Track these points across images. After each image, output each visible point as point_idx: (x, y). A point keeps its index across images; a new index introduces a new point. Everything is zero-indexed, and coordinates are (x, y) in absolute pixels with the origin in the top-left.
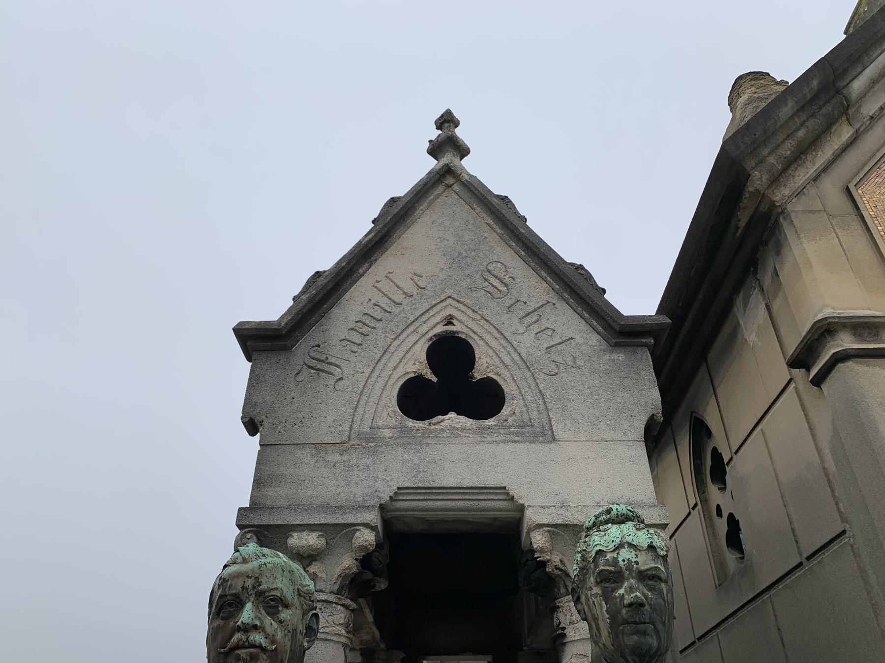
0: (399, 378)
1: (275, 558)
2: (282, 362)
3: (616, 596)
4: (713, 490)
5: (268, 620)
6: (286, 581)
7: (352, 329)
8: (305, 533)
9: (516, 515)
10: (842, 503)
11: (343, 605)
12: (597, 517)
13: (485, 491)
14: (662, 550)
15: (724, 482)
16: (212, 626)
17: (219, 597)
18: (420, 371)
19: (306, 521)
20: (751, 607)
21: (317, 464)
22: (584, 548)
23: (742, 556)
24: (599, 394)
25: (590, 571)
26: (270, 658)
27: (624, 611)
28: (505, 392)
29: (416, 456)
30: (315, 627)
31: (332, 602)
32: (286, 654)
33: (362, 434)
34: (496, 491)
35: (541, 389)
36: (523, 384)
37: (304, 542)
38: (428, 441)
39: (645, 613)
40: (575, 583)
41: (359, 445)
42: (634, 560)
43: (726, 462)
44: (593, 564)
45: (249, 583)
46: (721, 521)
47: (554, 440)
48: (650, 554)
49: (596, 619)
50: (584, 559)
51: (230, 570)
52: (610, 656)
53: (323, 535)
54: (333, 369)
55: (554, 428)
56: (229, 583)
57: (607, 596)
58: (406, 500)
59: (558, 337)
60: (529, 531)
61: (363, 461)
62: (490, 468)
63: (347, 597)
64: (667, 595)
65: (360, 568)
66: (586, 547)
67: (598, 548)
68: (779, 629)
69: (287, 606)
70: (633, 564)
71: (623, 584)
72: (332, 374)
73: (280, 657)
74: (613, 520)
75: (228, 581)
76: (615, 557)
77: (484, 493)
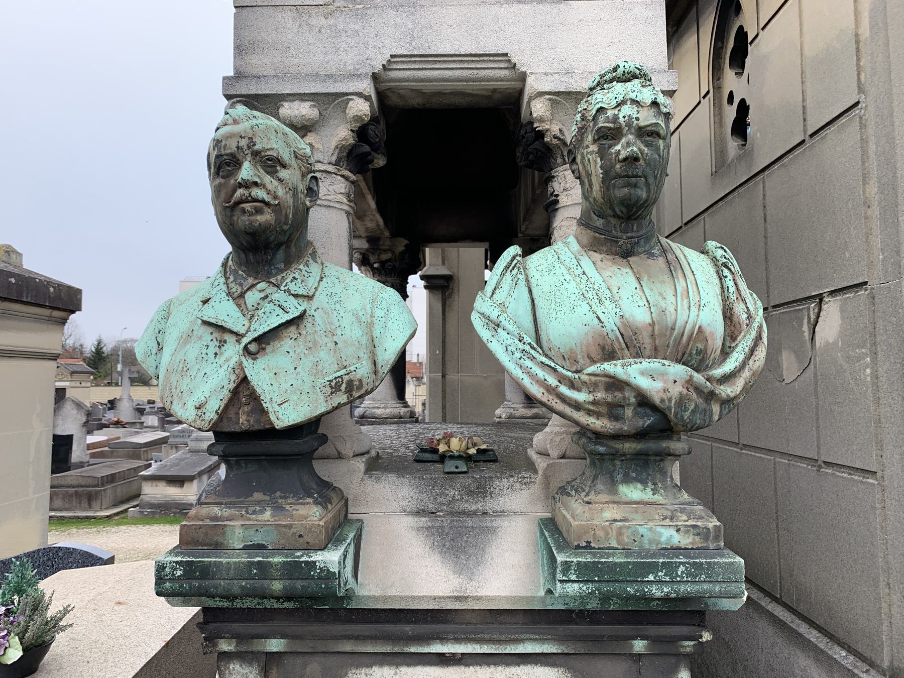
1: (266, 121)
3: (612, 153)
4: (729, 74)
5: (267, 179)
6: (281, 143)
8: (296, 102)
9: (517, 85)
10: (865, 73)
11: (342, 176)
12: (602, 76)
13: (485, 58)
14: (666, 107)
15: (742, 66)
16: (214, 184)
17: (216, 156)
20: (741, 190)
21: (300, 29)
22: (585, 107)
23: (743, 143)
25: (589, 129)
26: (274, 211)
27: (618, 166)
30: (315, 188)
31: (331, 173)
32: (290, 209)
37: (297, 112)
39: (639, 167)
40: (572, 144)
41: (345, 7)
42: (634, 116)
44: (593, 122)
45: (244, 143)
46: (730, 108)
49: (589, 175)
50: (584, 118)
51: (224, 130)
52: (599, 209)
53: (315, 106)
56: (223, 143)
57: (602, 153)
58: (400, 70)
60: (531, 99)
61: (351, 26)
63: (346, 169)
64: (663, 151)
65: (357, 139)
66: (587, 106)
67: (598, 106)
68: (765, 207)
69: (284, 166)
70: (633, 120)
71: (620, 139)
73: (284, 212)
74: (619, 78)
75: (221, 141)
76: (616, 113)
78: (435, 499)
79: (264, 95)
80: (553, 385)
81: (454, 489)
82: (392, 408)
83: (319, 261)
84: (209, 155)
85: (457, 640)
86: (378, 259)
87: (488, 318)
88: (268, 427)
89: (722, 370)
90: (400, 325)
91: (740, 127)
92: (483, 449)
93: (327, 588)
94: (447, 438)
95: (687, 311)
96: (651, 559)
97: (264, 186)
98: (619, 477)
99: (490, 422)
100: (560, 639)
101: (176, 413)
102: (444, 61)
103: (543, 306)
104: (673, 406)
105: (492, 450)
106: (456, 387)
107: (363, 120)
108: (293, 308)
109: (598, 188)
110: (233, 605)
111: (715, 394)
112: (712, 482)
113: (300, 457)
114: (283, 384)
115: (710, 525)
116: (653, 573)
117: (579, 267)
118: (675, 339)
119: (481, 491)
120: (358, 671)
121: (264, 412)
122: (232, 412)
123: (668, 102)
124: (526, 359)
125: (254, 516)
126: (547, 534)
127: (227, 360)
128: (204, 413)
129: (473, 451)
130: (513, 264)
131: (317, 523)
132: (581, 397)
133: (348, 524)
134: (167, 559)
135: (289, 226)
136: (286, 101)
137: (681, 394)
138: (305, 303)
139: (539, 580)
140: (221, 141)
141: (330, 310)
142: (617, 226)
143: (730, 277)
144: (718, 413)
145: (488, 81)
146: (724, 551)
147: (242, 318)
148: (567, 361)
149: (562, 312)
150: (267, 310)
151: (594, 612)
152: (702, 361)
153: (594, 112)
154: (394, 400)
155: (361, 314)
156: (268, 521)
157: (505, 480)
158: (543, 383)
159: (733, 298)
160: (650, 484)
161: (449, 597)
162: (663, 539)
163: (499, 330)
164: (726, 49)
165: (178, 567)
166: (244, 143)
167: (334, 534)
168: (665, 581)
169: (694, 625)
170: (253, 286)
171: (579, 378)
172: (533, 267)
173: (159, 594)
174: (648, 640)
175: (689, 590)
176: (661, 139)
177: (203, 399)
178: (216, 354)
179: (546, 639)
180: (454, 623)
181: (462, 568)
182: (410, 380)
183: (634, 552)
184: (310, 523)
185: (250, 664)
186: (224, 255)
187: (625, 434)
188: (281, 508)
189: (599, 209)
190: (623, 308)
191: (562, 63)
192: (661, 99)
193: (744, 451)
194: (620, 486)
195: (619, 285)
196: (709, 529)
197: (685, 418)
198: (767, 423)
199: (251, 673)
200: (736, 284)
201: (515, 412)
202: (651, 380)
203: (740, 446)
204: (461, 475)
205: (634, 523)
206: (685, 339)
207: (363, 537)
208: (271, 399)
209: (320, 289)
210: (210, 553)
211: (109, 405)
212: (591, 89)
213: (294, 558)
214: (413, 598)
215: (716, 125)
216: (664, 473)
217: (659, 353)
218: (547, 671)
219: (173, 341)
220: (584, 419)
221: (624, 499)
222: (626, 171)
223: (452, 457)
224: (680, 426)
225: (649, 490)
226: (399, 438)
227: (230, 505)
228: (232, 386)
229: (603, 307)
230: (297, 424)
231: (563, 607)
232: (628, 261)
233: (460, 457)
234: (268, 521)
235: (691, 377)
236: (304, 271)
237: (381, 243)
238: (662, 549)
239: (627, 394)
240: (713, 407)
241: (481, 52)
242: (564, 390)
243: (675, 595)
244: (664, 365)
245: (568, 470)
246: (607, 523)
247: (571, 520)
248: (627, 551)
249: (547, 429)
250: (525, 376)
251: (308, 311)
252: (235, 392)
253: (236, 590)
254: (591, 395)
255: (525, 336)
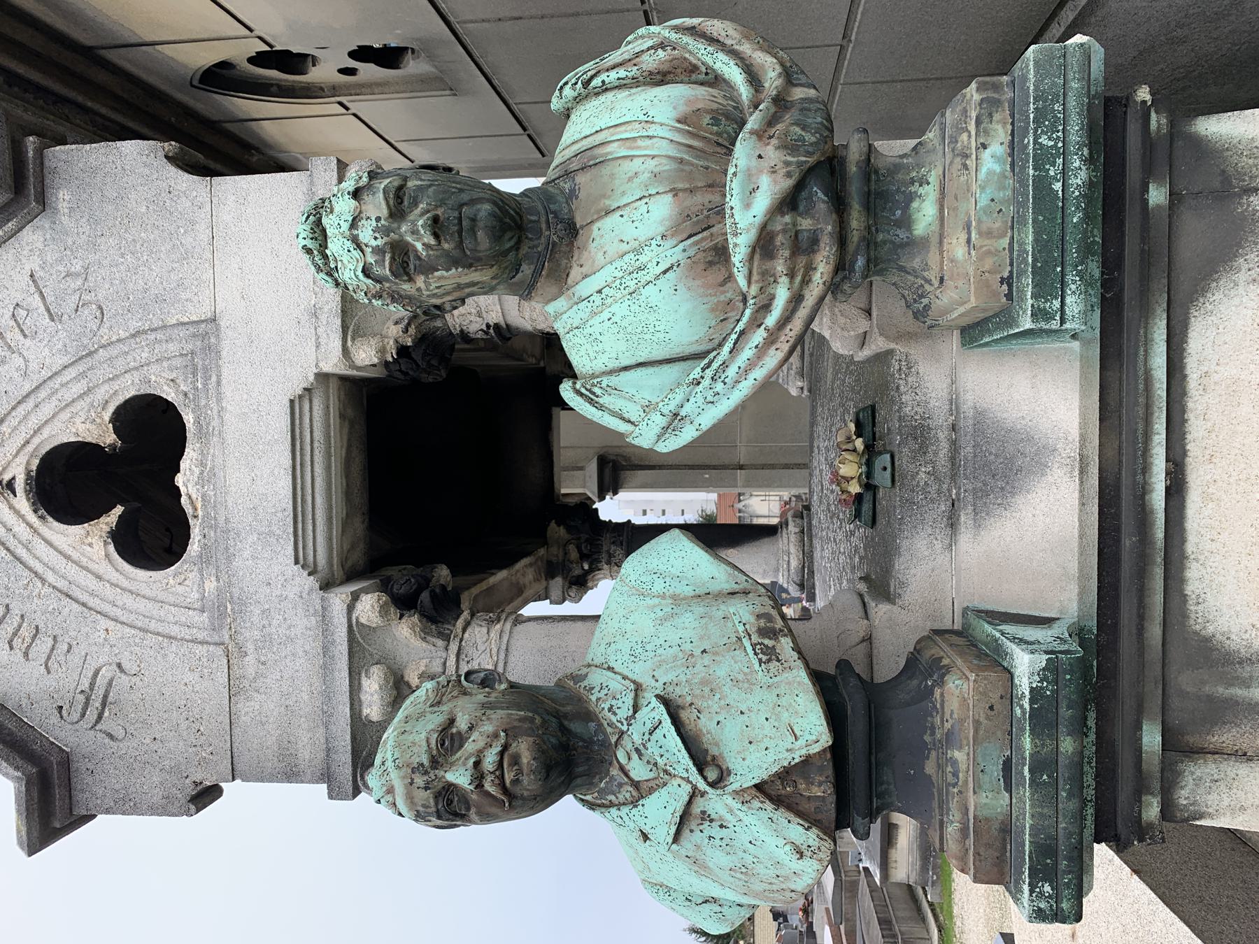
0: (117, 570)
1: (388, 746)
2: (89, 766)
4: (315, 75)
5: (470, 747)
7: (26, 654)
8: (363, 697)
9: (334, 385)
11: (464, 630)
12: (319, 270)
14: (360, 178)
15: (304, 57)
18: (104, 535)
19: (346, 698)
20: (476, 53)
23: (410, 51)
24: (134, 240)
25: (394, 288)
26: (515, 737)
27: (446, 246)
28: (137, 393)
29: (245, 539)
30: (482, 675)
31: (460, 647)
33: (213, 624)
34: (297, 415)
35: (127, 334)
36: (120, 364)
37: (376, 696)
38: (221, 520)
39: (446, 216)
42: (374, 223)
43: (268, 49)
45: (420, 780)
47: (215, 320)
48: (365, 197)
49: (459, 287)
50: (379, 296)
51: (402, 807)
52: (507, 271)
54: (101, 682)
55: (195, 318)
56: (421, 809)
58: (315, 551)
59: (30, 299)
61: (255, 619)
62: (261, 423)
63: (454, 626)
65: (412, 611)
67: (361, 276)
69: (452, 721)
71: (408, 243)
72: (110, 684)
73: (516, 724)
74: (320, 245)
75: (417, 811)
77: (301, 433)
78: (932, 501)
79: (352, 742)
80: (765, 335)
81: (917, 473)
82: (788, 542)
83: (584, 671)
84: (435, 827)
85: (1146, 469)
86: (577, 563)
87: (665, 429)
88: (829, 756)
89: (741, 87)
90: (677, 555)
91: (388, 57)
92: (856, 427)
93: (1071, 672)
94: (838, 479)
95: (655, 140)
96: (1028, 186)
97: (480, 751)
98: (902, 234)
99: (808, 403)
100: (1146, 313)
101: (808, 885)
102: (302, 489)
103: (647, 351)
104: (796, 159)
105: (857, 414)
106: (757, 449)
107: (386, 603)
108: (653, 714)
109: (478, 274)
110: (1090, 801)
111: (777, 96)
112: (896, 81)
113: (872, 706)
114: (766, 732)
115: (977, 97)
116: (1051, 184)
117: (591, 299)
118: (697, 157)
119: (920, 434)
120: (1193, 616)
121: (807, 761)
122: (807, 807)
123: (354, 175)
124: (726, 374)
125: (961, 775)
126: (987, 340)
127: (731, 811)
128: (809, 846)
129: (859, 444)
130: (587, 393)
131: (971, 684)
132: (782, 295)
133: (970, 631)
134: (1026, 905)
135: (536, 716)
136: (360, 711)
137: (779, 148)
138: (646, 695)
139: (1055, 349)
140: (417, 811)
141: (656, 659)
142: (531, 243)
143: (603, 76)
144: (806, 89)
145: (329, 426)
146: (1016, 75)
147: (669, 788)
148: (729, 315)
149: (657, 323)
150: (657, 751)
151: (1104, 265)
152: (728, 116)
153: (369, 281)
154: (777, 541)
155: (661, 614)
156: (968, 754)
157: (904, 398)
158: (762, 351)
159: (634, 71)
160: (913, 189)
161: (1081, 482)
162: (997, 168)
163: (683, 413)
164: (281, 80)
165: (1038, 890)
166: (420, 780)
167: (987, 655)
168: (1063, 164)
169: (1125, 113)
170: (622, 768)
171: (755, 297)
172: (590, 364)
173: (1078, 918)
174: (1148, 183)
175: (1077, 128)
176: (405, 185)
177: (788, 848)
178: (721, 826)
179: (1146, 337)
180: (1120, 473)
181: (1037, 462)
182: (743, 503)
183: (1018, 212)
184: (971, 693)
185: (1179, 774)
186: (579, 805)
187: (838, 229)
188: (949, 735)
189: (507, 271)
190: (650, 235)
191: (303, 322)
192: (349, 185)
193: (853, 38)
194: (916, 233)
195: (616, 241)
196: (982, 100)
197: (813, 139)
198: (813, 6)
199: (1193, 773)
200: (613, 67)
201: (794, 367)
202: (758, 193)
203: (845, 43)
204: (897, 463)
205: (972, 213)
206: (695, 143)
207: (990, 607)
208: (787, 750)
209: (626, 672)
210: (1016, 840)
211: (781, 920)
212: (337, 284)
213: (1025, 719)
214: (1081, 536)
215: (386, 90)
216: (896, 168)
217: (718, 180)
218: (1194, 333)
219: (703, 884)
220: (817, 289)
221: (935, 227)
222: (452, 235)
223: (869, 474)
224: (827, 147)
225: (921, 191)
226: (835, 541)
227: (943, 808)
228: (769, 806)
229: (650, 264)
230: (825, 712)
231: (1098, 312)
232: (582, 227)
233: (869, 464)
234: (968, 754)
235: (752, 132)
236: (600, 695)
237: (554, 559)
238: (1013, 170)
239: (779, 228)
240: (796, 98)
241: (289, 437)
242: (771, 320)
243: (1085, 149)
244: (735, 174)
245: (888, 304)
246: (973, 253)
247: (968, 306)
248: (1016, 223)
249: (827, 334)
250: (752, 376)
251: (658, 692)
252: (779, 801)
253: (1073, 805)
254: (781, 280)
255: (691, 377)
